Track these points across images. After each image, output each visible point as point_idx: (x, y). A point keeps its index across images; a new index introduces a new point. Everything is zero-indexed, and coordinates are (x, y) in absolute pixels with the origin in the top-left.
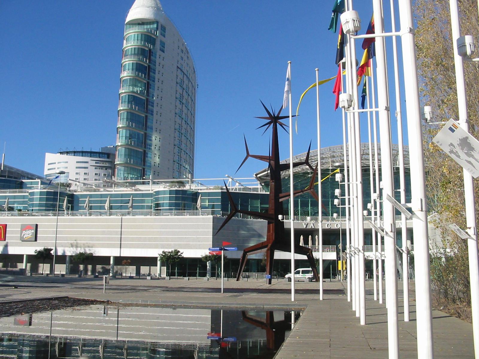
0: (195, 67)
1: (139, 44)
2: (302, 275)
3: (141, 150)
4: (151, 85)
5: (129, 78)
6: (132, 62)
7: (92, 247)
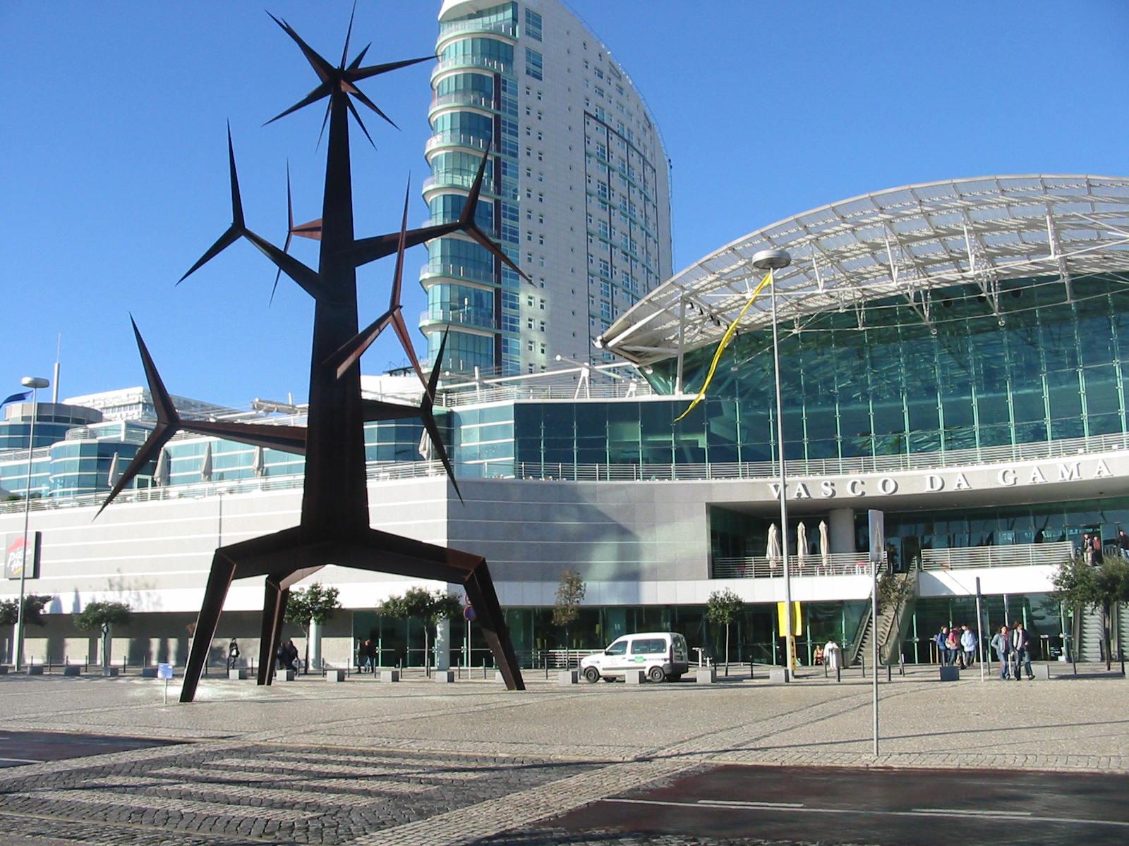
0: (648, 113)
1: (469, 62)
2: (633, 656)
3: (490, 335)
4: (505, 165)
5: (444, 152)
6: (450, 112)
7: (154, 588)
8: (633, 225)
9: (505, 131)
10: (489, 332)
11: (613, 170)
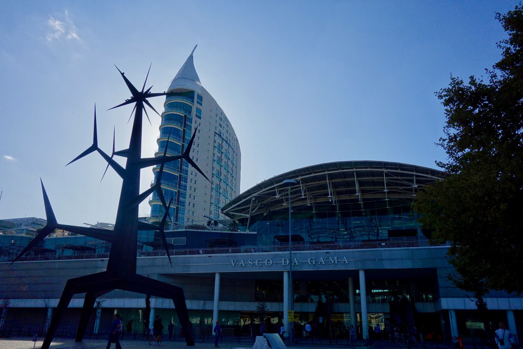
8: (228, 173)
9: (184, 165)
10: (177, 190)
11: (222, 166)
